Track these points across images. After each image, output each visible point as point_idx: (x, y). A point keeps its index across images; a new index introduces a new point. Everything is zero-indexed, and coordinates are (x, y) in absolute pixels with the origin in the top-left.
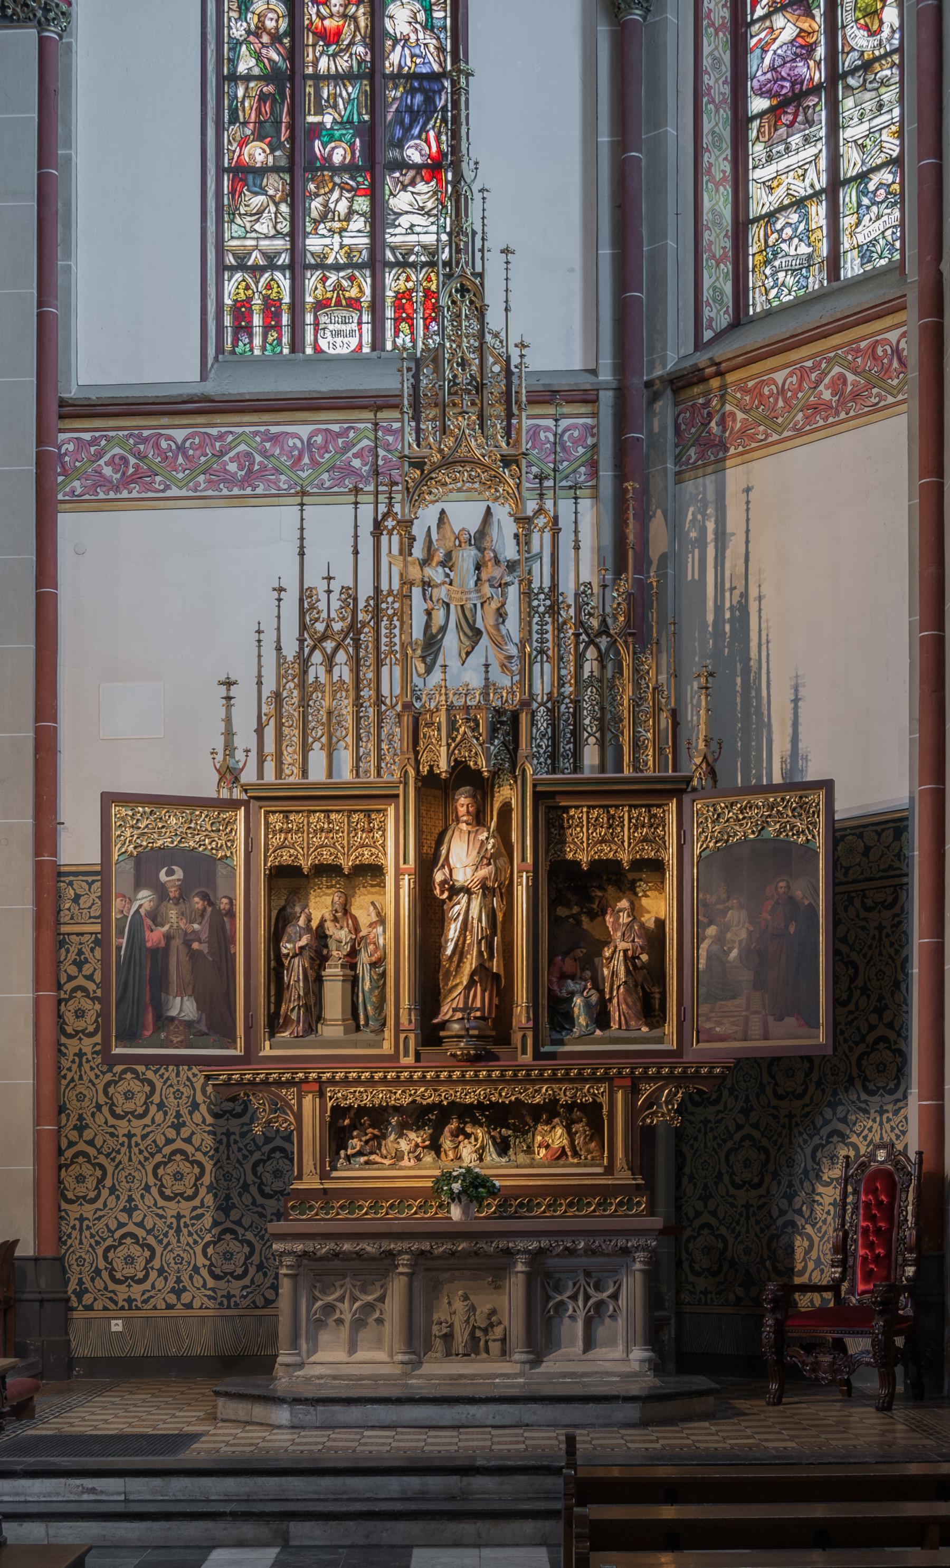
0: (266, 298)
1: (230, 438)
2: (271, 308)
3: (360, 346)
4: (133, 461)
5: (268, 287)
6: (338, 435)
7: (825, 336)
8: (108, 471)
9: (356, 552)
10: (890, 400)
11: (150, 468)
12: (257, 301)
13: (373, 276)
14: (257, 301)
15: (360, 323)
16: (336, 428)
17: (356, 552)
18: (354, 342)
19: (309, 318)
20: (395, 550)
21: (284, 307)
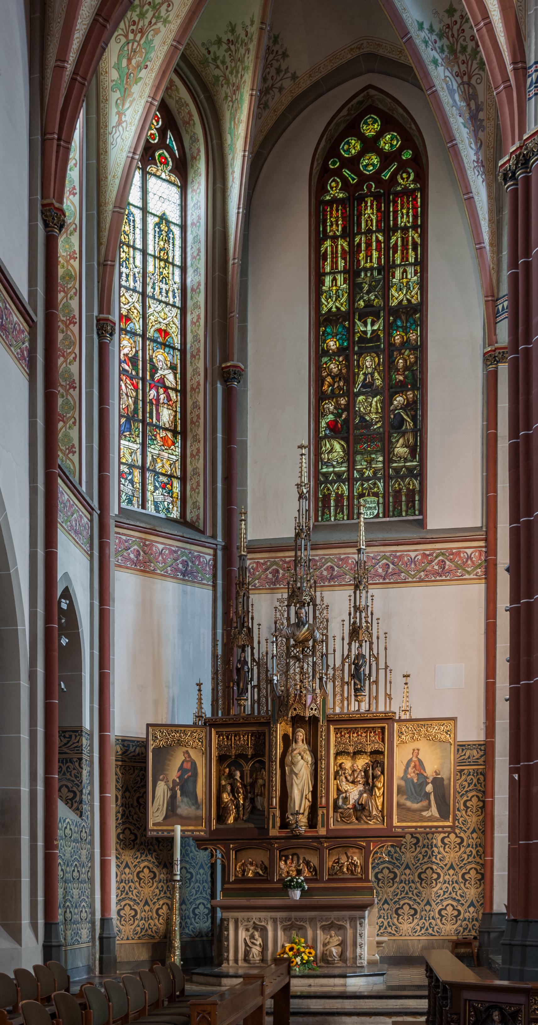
0: (337, 494)
1: (269, 564)
2: (339, 498)
3: (378, 513)
4: (391, 566)
5: (338, 489)
6: (263, 564)
7: (519, 504)
8: (325, 573)
9: (386, 649)
10: (410, 580)
11: (399, 570)
12: (333, 495)
13: (384, 482)
14: (333, 495)
15: (378, 504)
16: (262, 561)
17: (386, 649)
18: (376, 512)
19: (356, 502)
20: (331, 657)
21: (345, 498)
